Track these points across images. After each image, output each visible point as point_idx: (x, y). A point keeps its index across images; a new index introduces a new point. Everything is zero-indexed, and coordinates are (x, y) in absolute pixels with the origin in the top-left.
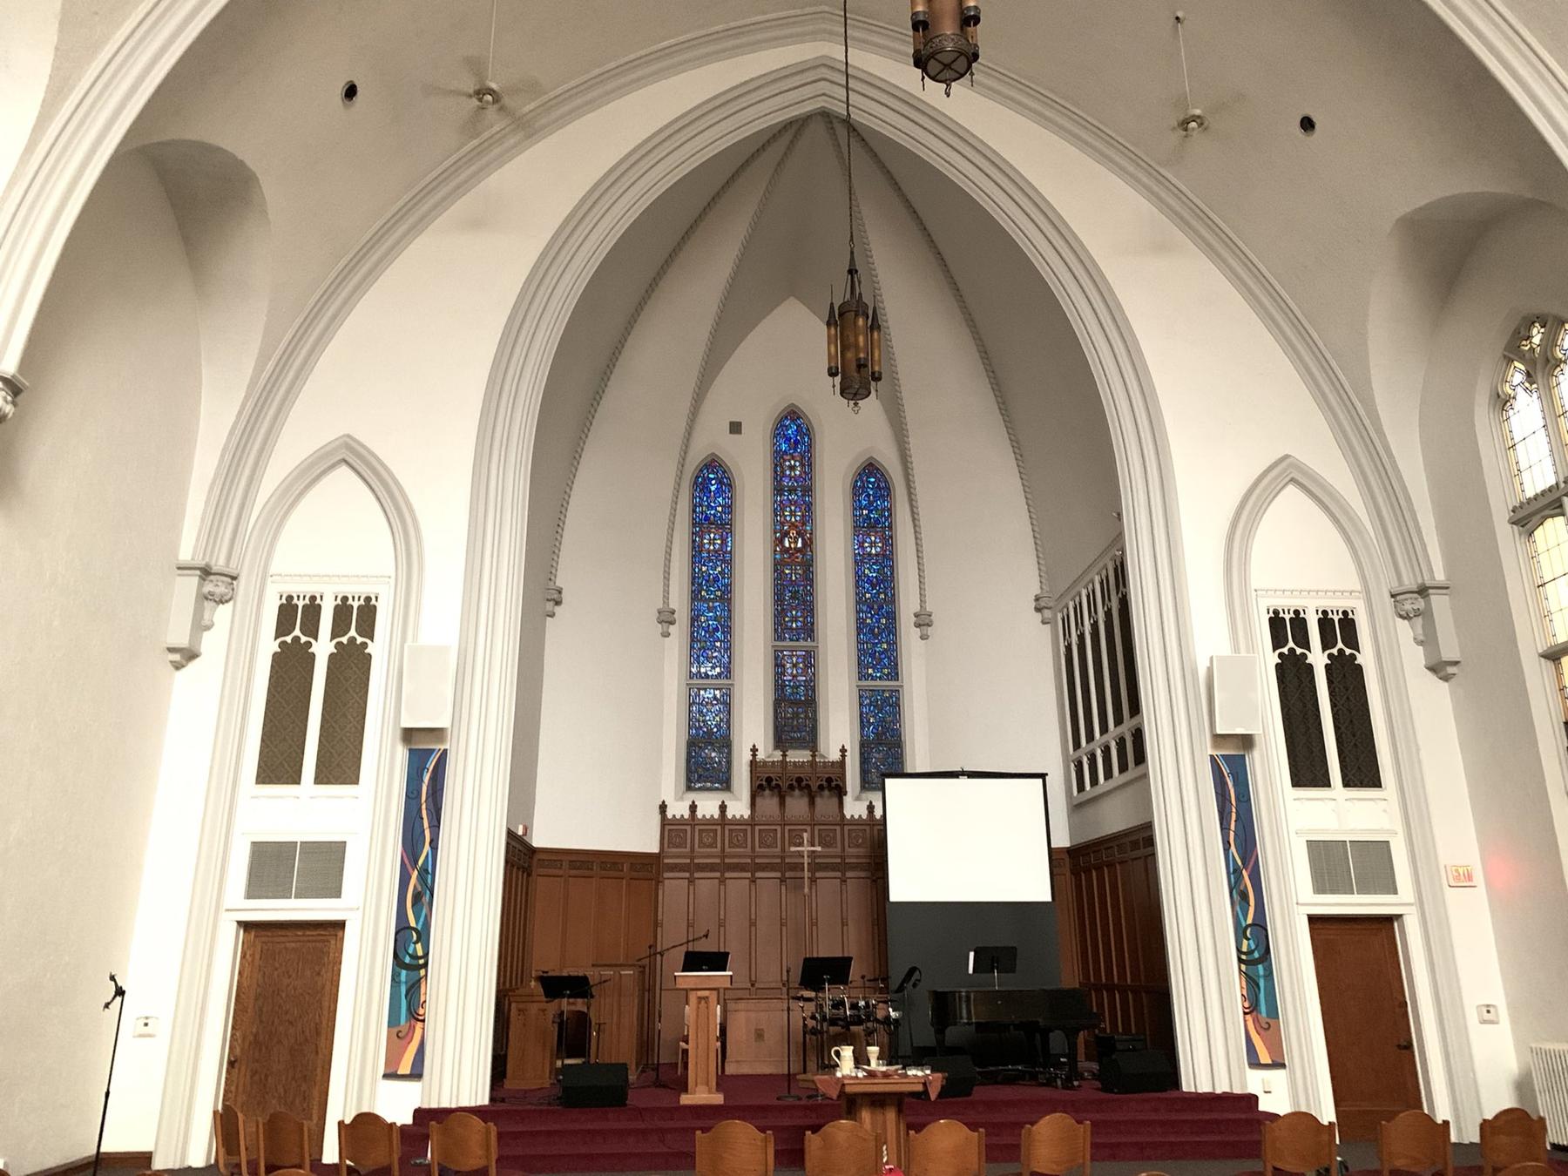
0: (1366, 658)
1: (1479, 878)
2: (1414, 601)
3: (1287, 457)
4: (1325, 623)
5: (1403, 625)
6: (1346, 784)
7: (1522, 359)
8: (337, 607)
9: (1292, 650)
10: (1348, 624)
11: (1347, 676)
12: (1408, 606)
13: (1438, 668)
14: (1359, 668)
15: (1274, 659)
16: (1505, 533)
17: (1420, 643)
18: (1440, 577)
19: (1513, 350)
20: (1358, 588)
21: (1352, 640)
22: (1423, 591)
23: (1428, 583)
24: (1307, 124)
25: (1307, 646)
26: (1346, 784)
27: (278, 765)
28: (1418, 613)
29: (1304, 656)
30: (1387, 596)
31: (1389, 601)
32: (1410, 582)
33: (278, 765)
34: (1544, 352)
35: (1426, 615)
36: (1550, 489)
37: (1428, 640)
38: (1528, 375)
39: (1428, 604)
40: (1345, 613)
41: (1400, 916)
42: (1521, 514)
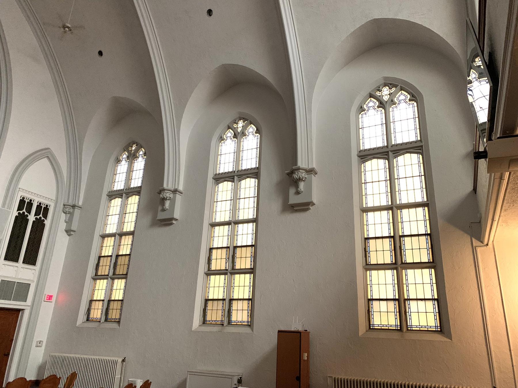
0: (47, 223)
1: (54, 299)
2: (70, 209)
3: (49, 148)
4: (39, 207)
5: (63, 215)
6: (24, 262)
7: (128, 152)
8: (21, 200)
9: (40, 218)
10: (46, 209)
11: (39, 226)
12: (67, 210)
13: (68, 232)
14: (44, 225)
15: (16, 213)
16: (104, 197)
17: (66, 222)
18: (80, 203)
19: (126, 148)
20: (54, 199)
21: (45, 216)
22: (74, 207)
23: (76, 205)
24: (100, 53)
25: (29, 212)
26: (24, 262)
27: (12, 255)
28: (69, 213)
29: (27, 216)
30: (62, 204)
31: (62, 206)
32: (71, 202)
33: (12, 255)
34: (134, 152)
35: (72, 214)
36: (121, 190)
37: (69, 222)
38: (128, 157)
39: (73, 212)
40: (31, 200)
41: (23, 310)
42: (111, 194)
